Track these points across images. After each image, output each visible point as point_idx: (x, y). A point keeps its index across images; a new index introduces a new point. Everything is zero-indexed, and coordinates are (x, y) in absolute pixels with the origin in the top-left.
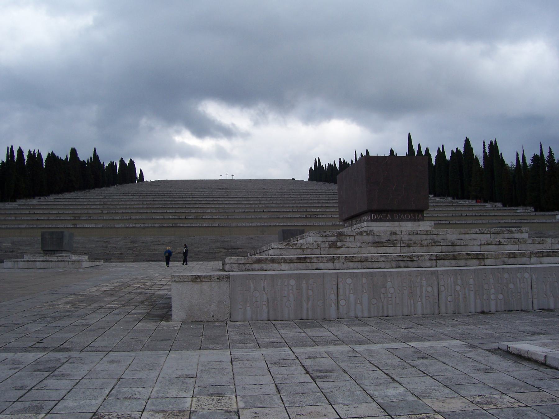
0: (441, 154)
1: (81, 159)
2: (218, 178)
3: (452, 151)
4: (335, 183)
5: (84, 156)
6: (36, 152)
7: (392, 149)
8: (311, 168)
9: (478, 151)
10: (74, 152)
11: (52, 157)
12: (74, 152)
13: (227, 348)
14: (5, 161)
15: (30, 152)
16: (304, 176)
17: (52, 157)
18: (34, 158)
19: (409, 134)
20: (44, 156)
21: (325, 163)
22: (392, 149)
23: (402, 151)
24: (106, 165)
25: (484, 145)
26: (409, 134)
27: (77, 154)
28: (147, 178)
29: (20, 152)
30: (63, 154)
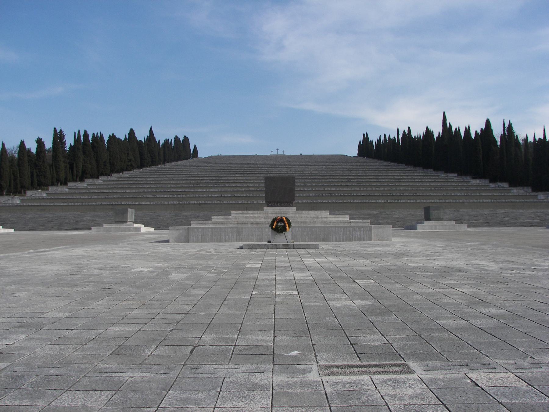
0: (467, 131)
1: (139, 139)
2: (269, 153)
3: (476, 132)
4: (359, 154)
5: (141, 135)
6: (99, 134)
7: (427, 128)
8: (360, 142)
9: (497, 132)
10: (132, 132)
11: (113, 138)
12: (132, 132)
13: (278, 385)
14: (73, 144)
15: (94, 135)
16: (354, 152)
17: (113, 138)
18: (98, 139)
19: (444, 113)
20: (106, 139)
21: (373, 138)
22: (427, 128)
23: (437, 130)
24: (162, 143)
25: (504, 125)
26: (444, 113)
27: (135, 134)
28: (202, 154)
29: (86, 135)
30: (122, 135)
